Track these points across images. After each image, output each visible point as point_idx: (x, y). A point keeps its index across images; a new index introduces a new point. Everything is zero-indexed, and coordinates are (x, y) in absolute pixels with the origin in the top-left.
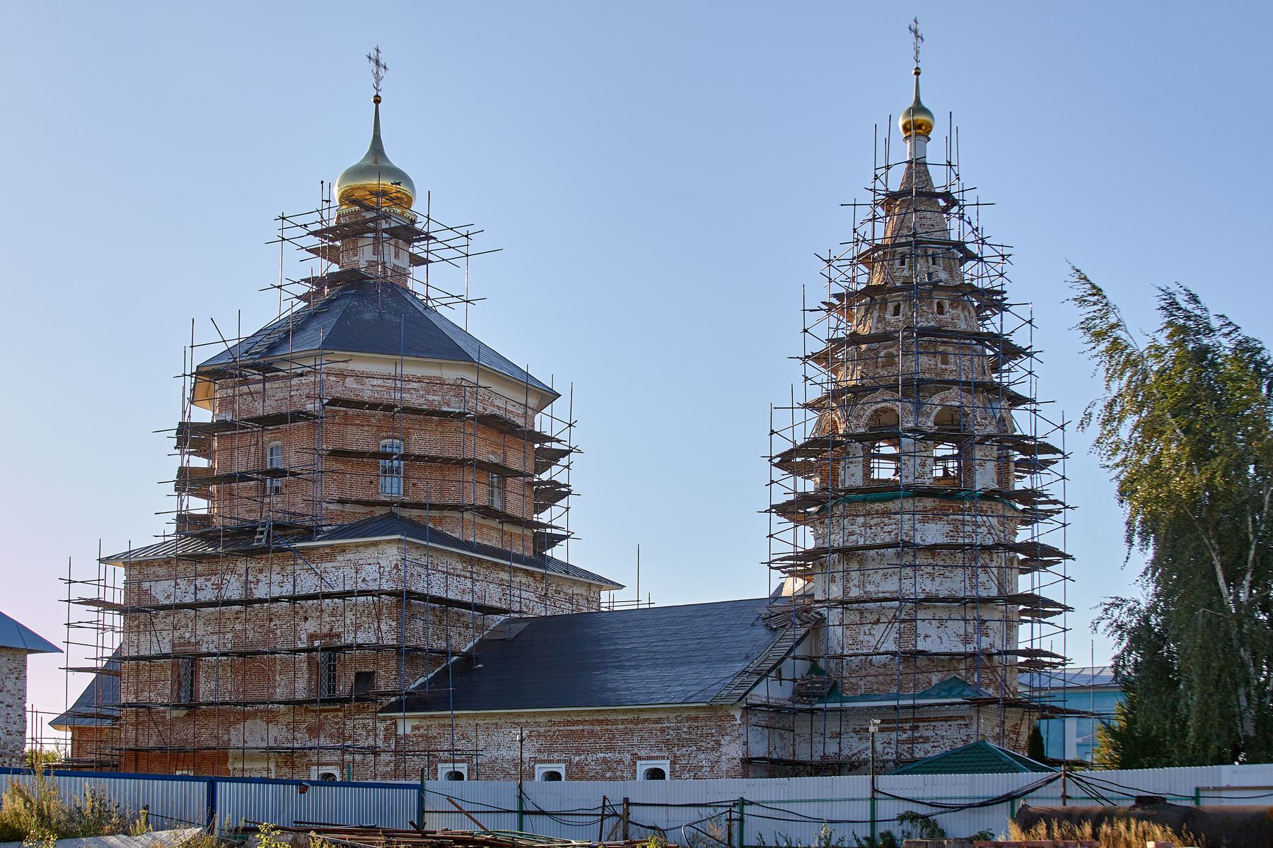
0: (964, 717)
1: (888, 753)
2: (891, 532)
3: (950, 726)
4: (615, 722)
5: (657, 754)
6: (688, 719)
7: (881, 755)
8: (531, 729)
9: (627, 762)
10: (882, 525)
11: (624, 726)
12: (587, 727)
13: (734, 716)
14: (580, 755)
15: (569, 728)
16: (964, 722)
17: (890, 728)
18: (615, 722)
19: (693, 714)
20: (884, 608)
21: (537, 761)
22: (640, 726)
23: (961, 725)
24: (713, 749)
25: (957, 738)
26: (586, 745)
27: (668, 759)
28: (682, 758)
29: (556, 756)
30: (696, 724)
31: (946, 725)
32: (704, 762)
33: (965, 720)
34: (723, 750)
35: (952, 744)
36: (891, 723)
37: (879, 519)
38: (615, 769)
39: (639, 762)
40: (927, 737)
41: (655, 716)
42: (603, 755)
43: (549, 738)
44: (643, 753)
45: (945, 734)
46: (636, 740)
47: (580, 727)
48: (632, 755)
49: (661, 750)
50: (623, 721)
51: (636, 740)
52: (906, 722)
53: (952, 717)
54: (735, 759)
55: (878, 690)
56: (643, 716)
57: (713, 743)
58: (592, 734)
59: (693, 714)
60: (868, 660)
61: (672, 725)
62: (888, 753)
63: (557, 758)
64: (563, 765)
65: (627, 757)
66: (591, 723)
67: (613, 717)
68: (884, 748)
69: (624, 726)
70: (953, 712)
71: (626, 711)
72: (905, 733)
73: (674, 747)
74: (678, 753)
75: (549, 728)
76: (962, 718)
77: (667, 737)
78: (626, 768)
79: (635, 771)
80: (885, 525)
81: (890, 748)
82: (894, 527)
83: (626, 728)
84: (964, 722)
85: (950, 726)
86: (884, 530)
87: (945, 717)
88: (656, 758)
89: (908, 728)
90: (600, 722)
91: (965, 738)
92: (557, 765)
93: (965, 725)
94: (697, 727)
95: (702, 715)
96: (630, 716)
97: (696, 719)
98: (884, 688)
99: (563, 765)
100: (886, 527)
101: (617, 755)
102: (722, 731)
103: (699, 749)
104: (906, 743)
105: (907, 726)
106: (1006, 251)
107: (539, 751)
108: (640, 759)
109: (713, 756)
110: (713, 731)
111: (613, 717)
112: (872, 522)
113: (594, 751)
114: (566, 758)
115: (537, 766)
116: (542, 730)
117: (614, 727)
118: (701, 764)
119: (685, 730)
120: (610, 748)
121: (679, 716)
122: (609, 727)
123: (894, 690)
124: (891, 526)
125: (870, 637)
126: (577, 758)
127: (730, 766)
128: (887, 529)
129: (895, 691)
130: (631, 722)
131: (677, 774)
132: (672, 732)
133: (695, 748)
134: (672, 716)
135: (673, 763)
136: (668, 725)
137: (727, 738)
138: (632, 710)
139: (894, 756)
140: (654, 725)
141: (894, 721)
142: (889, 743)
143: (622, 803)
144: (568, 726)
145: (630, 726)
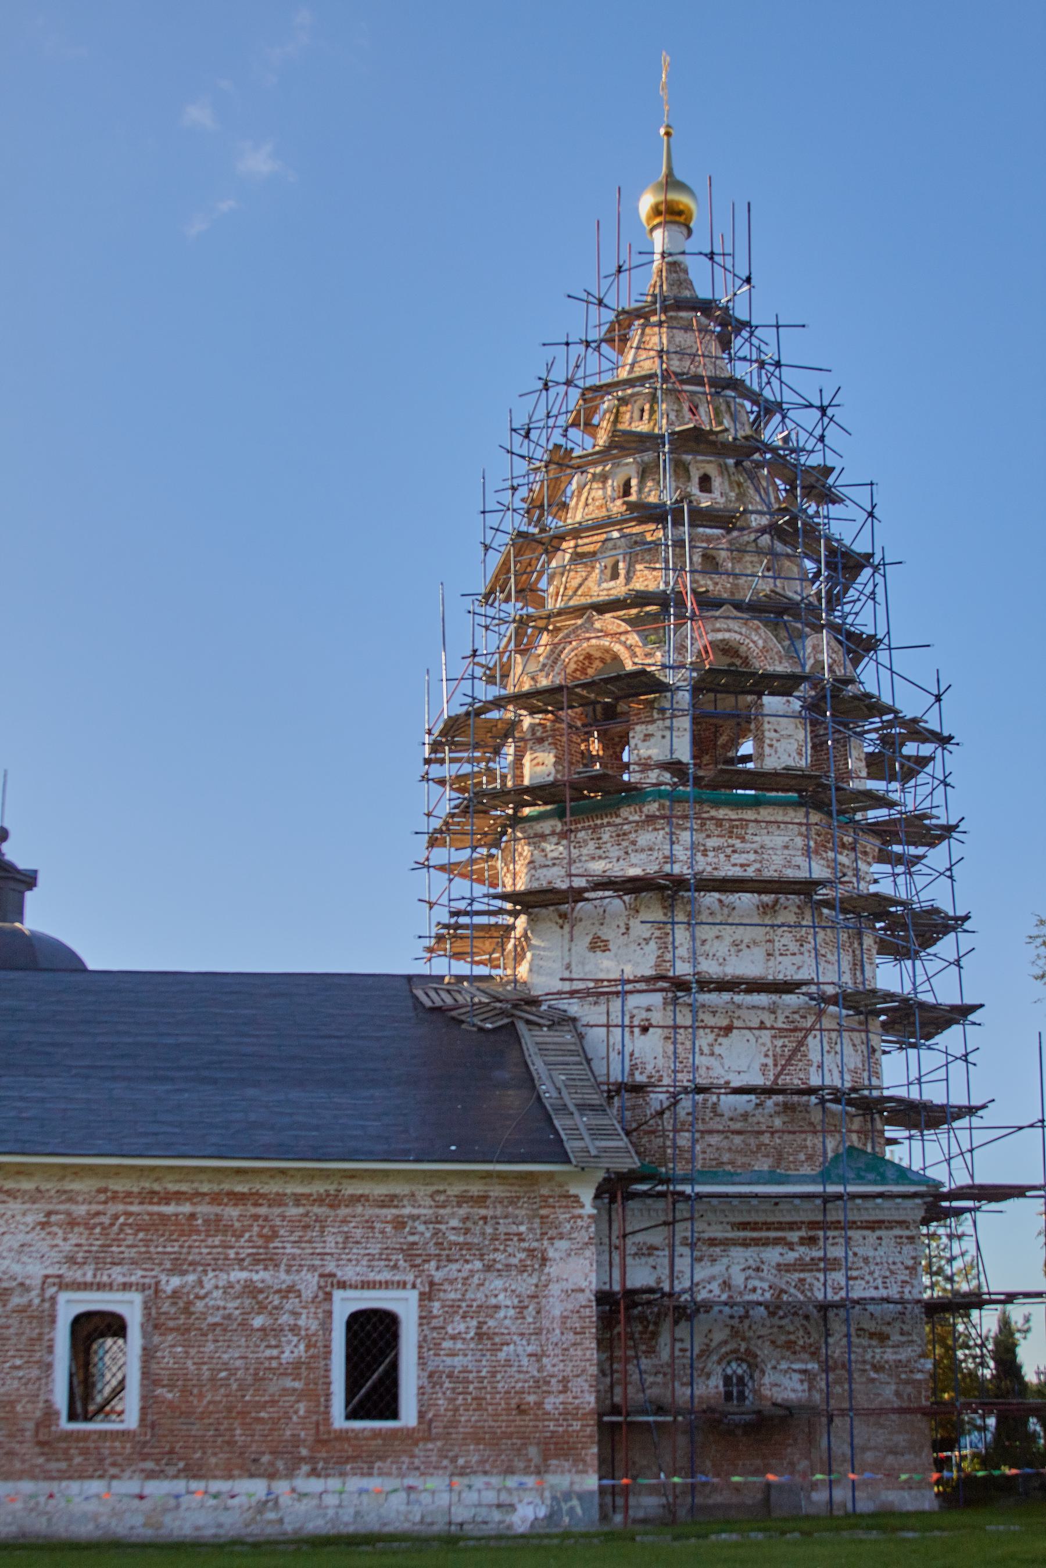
0: (904, 1222)
1: (754, 1290)
2: (748, 865)
3: (880, 1238)
4: (278, 1200)
5: (386, 1276)
6: (463, 1199)
7: (741, 1293)
8: (50, 1207)
9: (308, 1294)
10: (729, 851)
11: (301, 1210)
12: (204, 1209)
13: (576, 1196)
14: (183, 1273)
15: (156, 1208)
16: (907, 1233)
17: (760, 1239)
18: (278, 1200)
19: (475, 1189)
20: (739, 1006)
21: (63, 1285)
22: (343, 1211)
23: (901, 1237)
24: (522, 1269)
25: (894, 1263)
26: (203, 1248)
27: (414, 1286)
28: (446, 1286)
29: (117, 1275)
30: (483, 1212)
31: (872, 1236)
32: (501, 1297)
33: (908, 1228)
34: (552, 1270)
35: (888, 1274)
36: (761, 1229)
37: (722, 840)
38: (276, 1308)
39: (338, 1294)
40: (835, 1259)
41: (380, 1190)
42: (244, 1275)
43: (98, 1230)
44: (349, 1273)
45: (871, 1253)
46: (331, 1243)
47: (186, 1208)
48: (321, 1276)
49: (395, 1267)
50: (298, 1199)
51: (331, 1243)
52: (791, 1229)
53: (883, 1222)
54: (582, 1291)
55: (731, 1163)
56: (352, 1189)
57: (523, 1255)
58: (216, 1225)
59: (475, 1189)
60: (709, 1104)
61: (423, 1211)
62: (754, 1290)
63: (121, 1279)
64: (137, 1298)
65: (309, 1283)
66: (215, 1198)
67: (273, 1187)
68: (747, 1279)
69: (301, 1210)
70: (887, 1211)
71: (310, 1176)
72: (792, 1250)
73: (428, 1261)
74: (438, 1276)
75: (101, 1207)
76: (902, 1224)
77: (411, 1239)
78: (304, 1307)
79: (329, 1314)
80: (734, 852)
81: (762, 1279)
82: (752, 857)
83: (306, 1215)
84: (907, 1233)
85: (880, 1238)
86: (733, 860)
87: (867, 1222)
88: (386, 1285)
89: (796, 1240)
90: (238, 1198)
91: (910, 1263)
92: (119, 1296)
93: (908, 1238)
94: (484, 1218)
95: (497, 1191)
96: (318, 1188)
97: (481, 1200)
98: (744, 1160)
99: (137, 1298)
100: (736, 855)
101: (283, 1276)
102: (549, 1230)
103: (488, 1268)
104: (796, 1270)
105: (794, 1236)
106: (518, 442)
107: (71, 1260)
108: (343, 1285)
109: (525, 1284)
110: (523, 1229)
111: (273, 1187)
112: (711, 843)
113: (220, 1265)
114: (147, 1280)
115: (63, 1297)
116: (81, 1210)
117: (277, 1211)
118: (493, 1301)
119: (454, 1223)
120: (270, 1261)
121: (438, 1192)
122: (263, 1211)
123: (763, 1165)
124: (745, 856)
125: (712, 1059)
126: (176, 1281)
127: (570, 1307)
128: (736, 858)
129: (766, 1168)
130: (320, 1200)
131: (435, 1323)
132: (421, 1228)
133: (478, 1265)
134: (422, 1191)
135: (426, 1297)
136: (416, 1211)
137: (563, 1245)
138: (326, 1174)
139: (768, 1295)
140: (378, 1211)
141: (768, 1226)
142: (758, 1269)
143: (848, 1419)
144: (151, 1203)
145: (316, 1210)
